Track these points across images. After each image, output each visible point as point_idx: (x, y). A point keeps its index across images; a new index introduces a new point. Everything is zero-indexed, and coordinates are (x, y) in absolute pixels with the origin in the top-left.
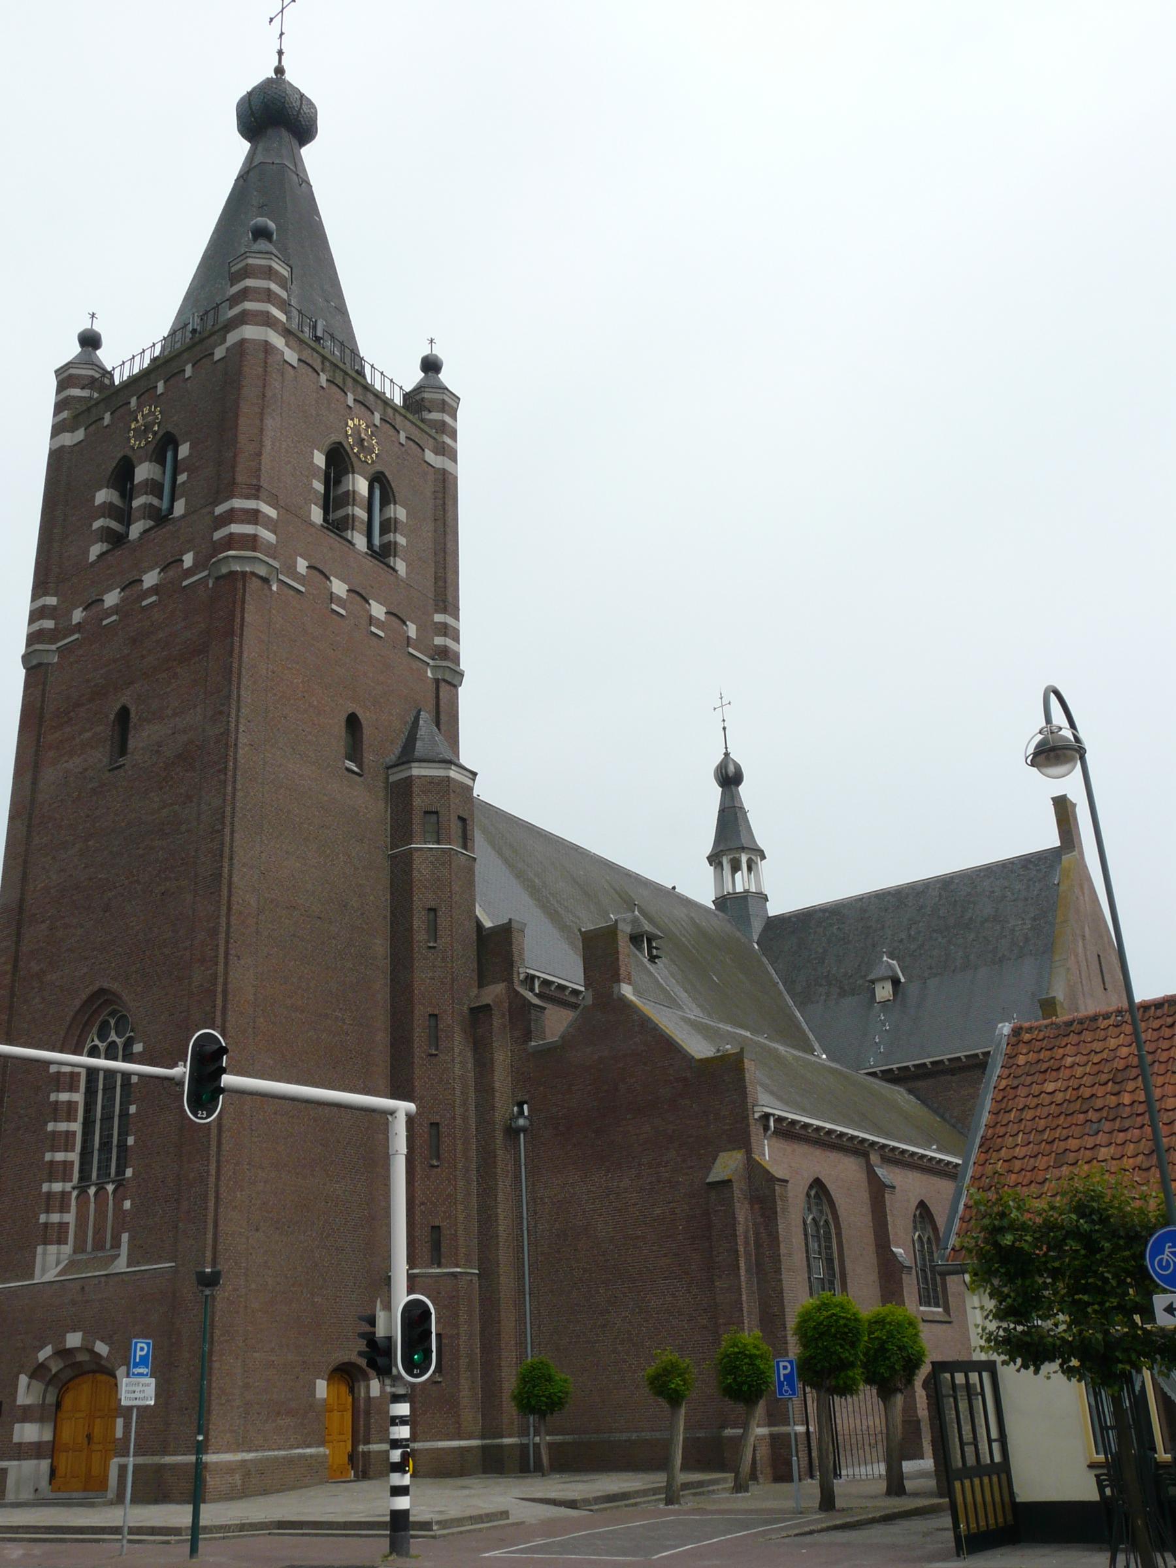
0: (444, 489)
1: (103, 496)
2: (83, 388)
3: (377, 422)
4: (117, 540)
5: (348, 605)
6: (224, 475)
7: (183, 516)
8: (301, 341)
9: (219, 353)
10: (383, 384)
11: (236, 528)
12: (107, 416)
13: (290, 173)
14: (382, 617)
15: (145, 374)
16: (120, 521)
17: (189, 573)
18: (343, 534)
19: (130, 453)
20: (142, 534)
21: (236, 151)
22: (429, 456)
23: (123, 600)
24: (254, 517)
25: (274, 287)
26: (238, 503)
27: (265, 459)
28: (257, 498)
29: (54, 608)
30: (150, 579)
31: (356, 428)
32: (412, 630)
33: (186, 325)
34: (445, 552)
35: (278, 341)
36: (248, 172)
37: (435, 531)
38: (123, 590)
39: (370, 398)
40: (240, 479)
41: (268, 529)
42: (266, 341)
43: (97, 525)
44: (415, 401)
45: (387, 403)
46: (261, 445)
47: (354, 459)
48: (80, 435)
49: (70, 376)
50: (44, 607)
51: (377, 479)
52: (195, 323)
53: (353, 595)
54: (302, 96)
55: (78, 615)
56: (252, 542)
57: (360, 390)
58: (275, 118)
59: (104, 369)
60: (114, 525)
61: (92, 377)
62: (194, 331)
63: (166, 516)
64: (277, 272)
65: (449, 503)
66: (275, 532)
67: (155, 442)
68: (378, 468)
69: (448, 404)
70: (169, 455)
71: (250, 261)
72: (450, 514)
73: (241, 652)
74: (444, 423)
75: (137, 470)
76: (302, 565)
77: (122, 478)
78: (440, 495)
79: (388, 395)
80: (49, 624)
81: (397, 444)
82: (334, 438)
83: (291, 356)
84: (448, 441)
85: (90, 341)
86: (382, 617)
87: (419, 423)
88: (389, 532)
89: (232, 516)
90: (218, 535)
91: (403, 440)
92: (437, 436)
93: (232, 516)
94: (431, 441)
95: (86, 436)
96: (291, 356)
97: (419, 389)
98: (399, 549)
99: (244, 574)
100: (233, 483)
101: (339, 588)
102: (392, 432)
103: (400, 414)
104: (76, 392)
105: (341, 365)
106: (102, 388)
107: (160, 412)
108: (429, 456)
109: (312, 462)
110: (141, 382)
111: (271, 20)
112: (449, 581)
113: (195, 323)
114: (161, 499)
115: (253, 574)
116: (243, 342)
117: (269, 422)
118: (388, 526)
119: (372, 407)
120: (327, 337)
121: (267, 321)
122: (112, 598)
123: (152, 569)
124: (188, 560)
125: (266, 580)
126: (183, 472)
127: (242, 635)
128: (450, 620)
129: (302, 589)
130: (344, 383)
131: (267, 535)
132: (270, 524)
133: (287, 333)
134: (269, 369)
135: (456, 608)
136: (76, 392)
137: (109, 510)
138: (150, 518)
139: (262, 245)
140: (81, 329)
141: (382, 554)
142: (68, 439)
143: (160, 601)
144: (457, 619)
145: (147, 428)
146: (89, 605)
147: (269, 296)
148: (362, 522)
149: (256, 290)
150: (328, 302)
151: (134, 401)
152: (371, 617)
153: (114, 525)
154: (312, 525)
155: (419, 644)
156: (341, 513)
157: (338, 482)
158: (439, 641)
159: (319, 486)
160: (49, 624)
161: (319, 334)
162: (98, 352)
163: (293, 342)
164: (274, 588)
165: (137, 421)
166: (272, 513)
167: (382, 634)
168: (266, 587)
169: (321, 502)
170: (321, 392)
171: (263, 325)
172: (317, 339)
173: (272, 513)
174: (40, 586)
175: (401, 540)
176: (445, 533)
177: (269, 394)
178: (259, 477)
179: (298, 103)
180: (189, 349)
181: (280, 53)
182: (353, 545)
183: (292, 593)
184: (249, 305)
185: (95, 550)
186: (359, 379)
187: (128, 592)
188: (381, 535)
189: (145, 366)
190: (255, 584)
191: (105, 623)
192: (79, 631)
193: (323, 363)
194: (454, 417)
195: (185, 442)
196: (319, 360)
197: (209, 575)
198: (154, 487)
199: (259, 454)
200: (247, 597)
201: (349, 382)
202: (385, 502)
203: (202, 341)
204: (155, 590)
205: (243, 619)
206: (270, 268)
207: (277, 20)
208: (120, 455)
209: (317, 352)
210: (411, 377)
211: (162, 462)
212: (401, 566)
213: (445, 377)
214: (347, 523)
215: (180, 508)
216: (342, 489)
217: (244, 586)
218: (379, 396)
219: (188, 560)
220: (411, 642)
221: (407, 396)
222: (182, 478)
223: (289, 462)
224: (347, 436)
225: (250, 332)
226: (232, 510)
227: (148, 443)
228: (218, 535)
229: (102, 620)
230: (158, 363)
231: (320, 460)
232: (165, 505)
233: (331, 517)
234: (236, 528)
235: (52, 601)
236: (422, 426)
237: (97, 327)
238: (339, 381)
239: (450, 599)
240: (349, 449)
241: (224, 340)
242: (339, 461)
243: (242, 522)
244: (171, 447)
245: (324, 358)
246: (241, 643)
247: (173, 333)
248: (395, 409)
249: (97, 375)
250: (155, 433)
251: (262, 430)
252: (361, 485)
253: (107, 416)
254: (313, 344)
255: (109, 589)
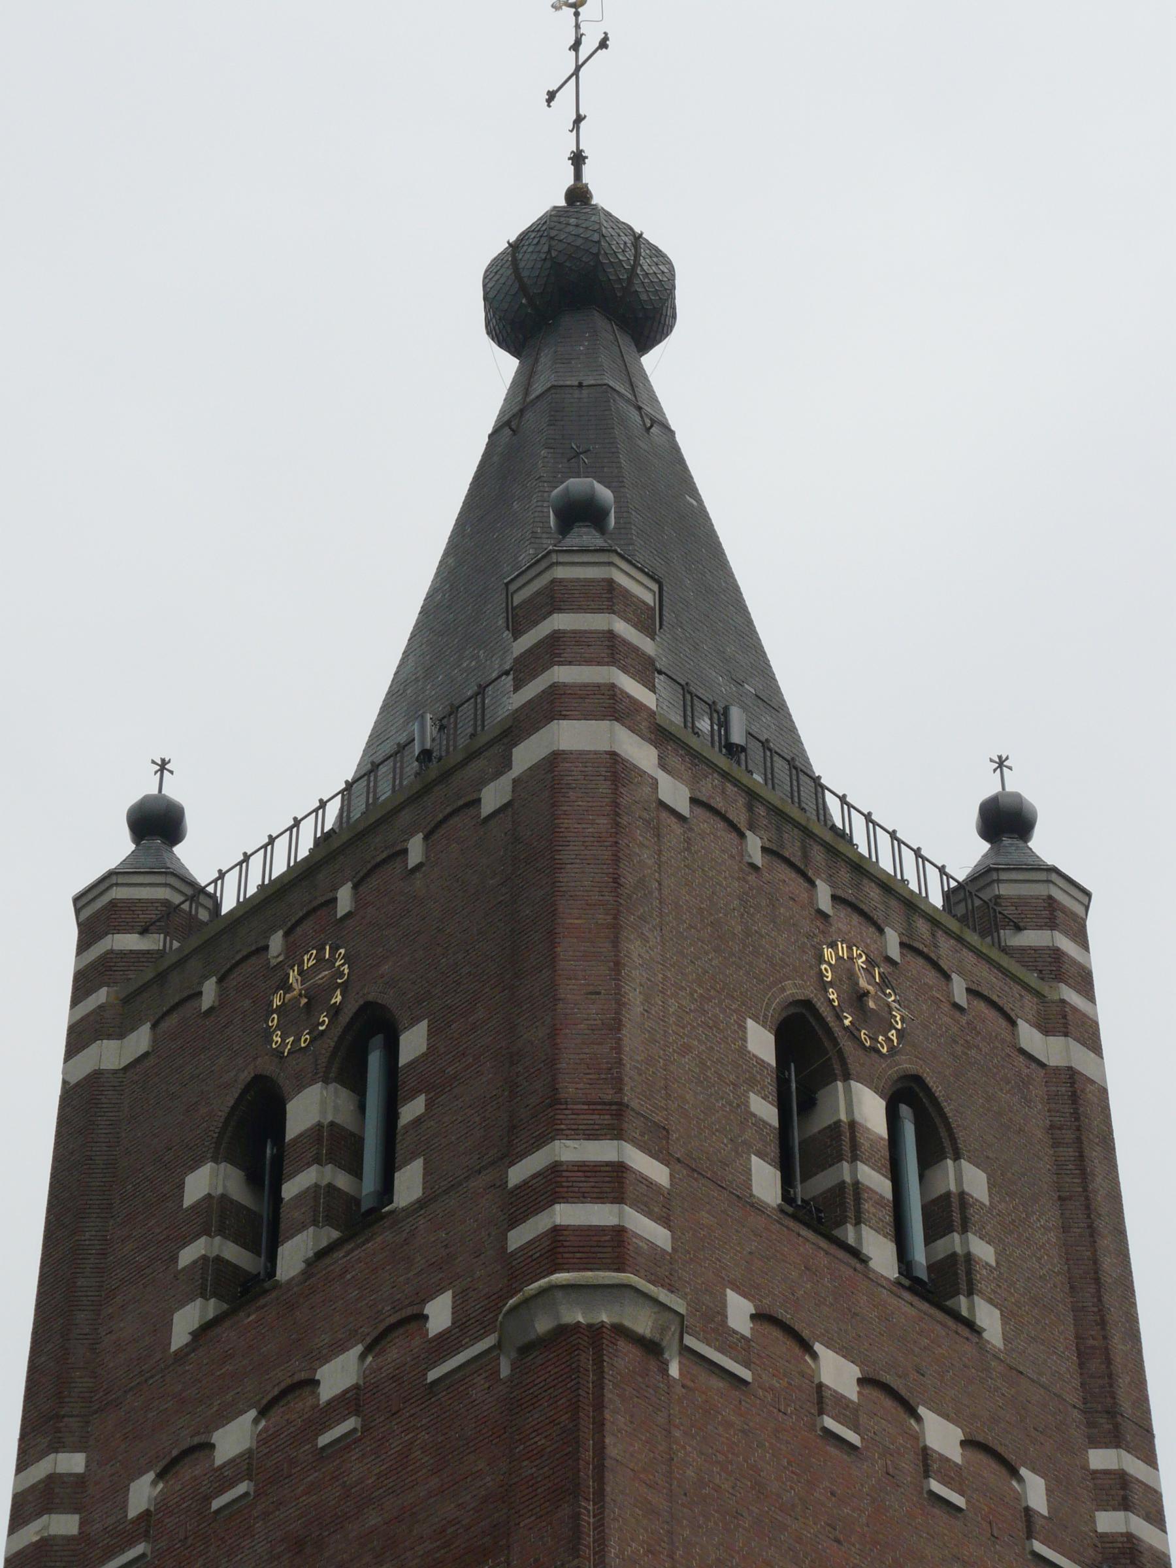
0: (1076, 1123)
1: (201, 1183)
2: (144, 932)
3: (894, 952)
4: (240, 1290)
5: (863, 1419)
6: (531, 1092)
7: (421, 1205)
8: (695, 756)
9: (493, 796)
10: (897, 859)
11: (566, 1214)
12: (210, 992)
13: (622, 404)
14: (955, 1454)
15: (303, 875)
16: (252, 1246)
17: (446, 1344)
18: (837, 1233)
19: (266, 1066)
20: (309, 1263)
21: (491, 375)
22: (1030, 1037)
23: (263, 1440)
24: (612, 1182)
25: (622, 628)
26: (570, 1151)
27: (632, 1039)
28: (617, 1133)
29: (80, 1481)
30: (338, 1375)
31: (845, 968)
32: (1035, 1492)
33: (402, 748)
34: (1097, 1281)
35: (642, 754)
36: (522, 412)
37: (1065, 1229)
38: (263, 1413)
39: (870, 892)
40: (570, 1089)
41: (649, 1214)
42: (613, 754)
43: (188, 1255)
44: (977, 903)
45: (912, 905)
46: (620, 1004)
47: (847, 1045)
48: (140, 1040)
49: (113, 904)
50: (52, 1480)
51: (906, 1094)
52: (425, 733)
53: (875, 1394)
54: (638, 238)
55: (142, 1494)
56: (612, 1246)
57: (844, 875)
58: (576, 295)
59: (192, 884)
60: (232, 1252)
61: (166, 903)
62: (426, 755)
63: (371, 1211)
64: (626, 593)
65: (1094, 1154)
66: (665, 1221)
67: (337, 1031)
68: (906, 1064)
69: (1061, 906)
70: (375, 1060)
71: (561, 573)
72: (1098, 1182)
73: (601, 1542)
74: (1057, 955)
75: (291, 1107)
76: (739, 1312)
77: (255, 1132)
78: (1069, 1136)
79: (913, 886)
80: (65, 1524)
81: (946, 1007)
82: (793, 990)
83: (674, 792)
84: (1074, 998)
85: (157, 824)
86: (955, 1454)
87: (995, 954)
88: (949, 1229)
89: (556, 1184)
90: (519, 1237)
91: (961, 997)
92: (1044, 988)
93: (556, 1184)
94: (1029, 1002)
95: (155, 1041)
96: (674, 792)
97: (983, 875)
98: (981, 1274)
99: (595, 1332)
100: (554, 1100)
101: (837, 1372)
102: (931, 976)
103: (949, 933)
104: (129, 942)
105: (795, 813)
106: (191, 925)
107: (347, 958)
108: (1030, 1037)
109: (743, 1051)
110: (293, 898)
111: (551, 96)
112: (1118, 1359)
113: (425, 733)
114: (356, 1170)
115: (620, 1330)
116: (555, 759)
117: (635, 949)
118: (945, 1215)
119: (878, 916)
120: (755, 750)
121: (612, 706)
122: (234, 1439)
123: (339, 1347)
124: (440, 1314)
125: (652, 1348)
126: (412, 1097)
127: (600, 1494)
128: (1134, 1466)
129: (745, 1374)
130: (805, 856)
131: (649, 1230)
132: (651, 1201)
133: (660, 735)
134: (624, 821)
135: (1147, 1433)
136: (129, 942)
137: (216, 1215)
138: (330, 1221)
139: (584, 536)
140: (134, 798)
141: (939, 1287)
142: (111, 1055)
143: (366, 1428)
144: (1150, 1458)
145: (315, 999)
146: (175, 1462)
147: (612, 650)
148: (880, 1201)
149: (580, 638)
150: (740, 684)
151: (276, 943)
152: (925, 1454)
153: (232, 1252)
154: (757, 1207)
155: (1057, 1528)
156: (822, 1182)
157: (808, 1104)
158: (1109, 1522)
159: (765, 1110)
160: (65, 1524)
161: (737, 737)
162: (178, 850)
163: (674, 761)
164: (674, 1370)
165: (288, 988)
166: (657, 1172)
167: (959, 1500)
168: (653, 1365)
169: (774, 1150)
170: (752, 878)
171: (603, 718)
172: (733, 750)
173: (657, 1172)
174: (41, 1428)
175: (983, 1251)
176: (1092, 1231)
177: (629, 879)
178: (618, 1084)
179: (630, 254)
180: (416, 798)
181: (578, 159)
182: (864, 1260)
183: (717, 1383)
184: (563, 674)
185: (185, 1322)
186: (842, 847)
187: (277, 1415)
188: (929, 1239)
189: (303, 853)
190: (625, 1358)
191: (216, 1504)
192: (146, 1536)
193: (750, 808)
194: (1080, 936)
195: (415, 1021)
196: (741, 801)
197: (498, 1346)
198: (338, 1145)
199: (616, 1025)
200: (609, 1394)
201: (818, 855)
202: (929, 1157)
203: (445, 776)
204: (350, 1401)
205: (600, 1450)
206: (610, 584)
207: (566, 97)
208: (246, 1076)
209: (736, 783)
210: (965, 852)
211: (354, 1080)
212: (988, 1318)
213: (1044, 844)
214: (843, 1204)
215: (409, 1184)
216: (821, 1121)
217: (599, 1362)
218: (890, 887)
219: (440, 1314)
220: (1039, 1523)
221: (955, 895)
222: (411, 1110)
223: (686, 1049)
224: (824, 986)
225: (572, 735)
226: (555, 1169)
227: (317, 1037)
228: (519, 1237)
229: (208, 1499)
230: (336, 843)
231: (761, 1043)
232: (370, 1183)
233: (800, 1191)
234: (566, 1214)
235: (73, 1463)
236: (1005, 961)
237: (174, 790)
238: (792, 850)
239: (1126, 1407)
240: (830, 1019)
241: (507, 764)
242: (809, 1050)
243: (582, 1197)
244: (378, 1040)
245: (752, 796)
246: (600, 1515)
247: (369, 771)
248: (932, 920)
249: (177, 899)
250: (335, 1011)
251: (617, 966)
252: (870, 1110)
253: (210, 992)
254: (722, 762)
255: (225, 1417)
